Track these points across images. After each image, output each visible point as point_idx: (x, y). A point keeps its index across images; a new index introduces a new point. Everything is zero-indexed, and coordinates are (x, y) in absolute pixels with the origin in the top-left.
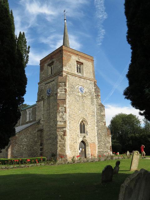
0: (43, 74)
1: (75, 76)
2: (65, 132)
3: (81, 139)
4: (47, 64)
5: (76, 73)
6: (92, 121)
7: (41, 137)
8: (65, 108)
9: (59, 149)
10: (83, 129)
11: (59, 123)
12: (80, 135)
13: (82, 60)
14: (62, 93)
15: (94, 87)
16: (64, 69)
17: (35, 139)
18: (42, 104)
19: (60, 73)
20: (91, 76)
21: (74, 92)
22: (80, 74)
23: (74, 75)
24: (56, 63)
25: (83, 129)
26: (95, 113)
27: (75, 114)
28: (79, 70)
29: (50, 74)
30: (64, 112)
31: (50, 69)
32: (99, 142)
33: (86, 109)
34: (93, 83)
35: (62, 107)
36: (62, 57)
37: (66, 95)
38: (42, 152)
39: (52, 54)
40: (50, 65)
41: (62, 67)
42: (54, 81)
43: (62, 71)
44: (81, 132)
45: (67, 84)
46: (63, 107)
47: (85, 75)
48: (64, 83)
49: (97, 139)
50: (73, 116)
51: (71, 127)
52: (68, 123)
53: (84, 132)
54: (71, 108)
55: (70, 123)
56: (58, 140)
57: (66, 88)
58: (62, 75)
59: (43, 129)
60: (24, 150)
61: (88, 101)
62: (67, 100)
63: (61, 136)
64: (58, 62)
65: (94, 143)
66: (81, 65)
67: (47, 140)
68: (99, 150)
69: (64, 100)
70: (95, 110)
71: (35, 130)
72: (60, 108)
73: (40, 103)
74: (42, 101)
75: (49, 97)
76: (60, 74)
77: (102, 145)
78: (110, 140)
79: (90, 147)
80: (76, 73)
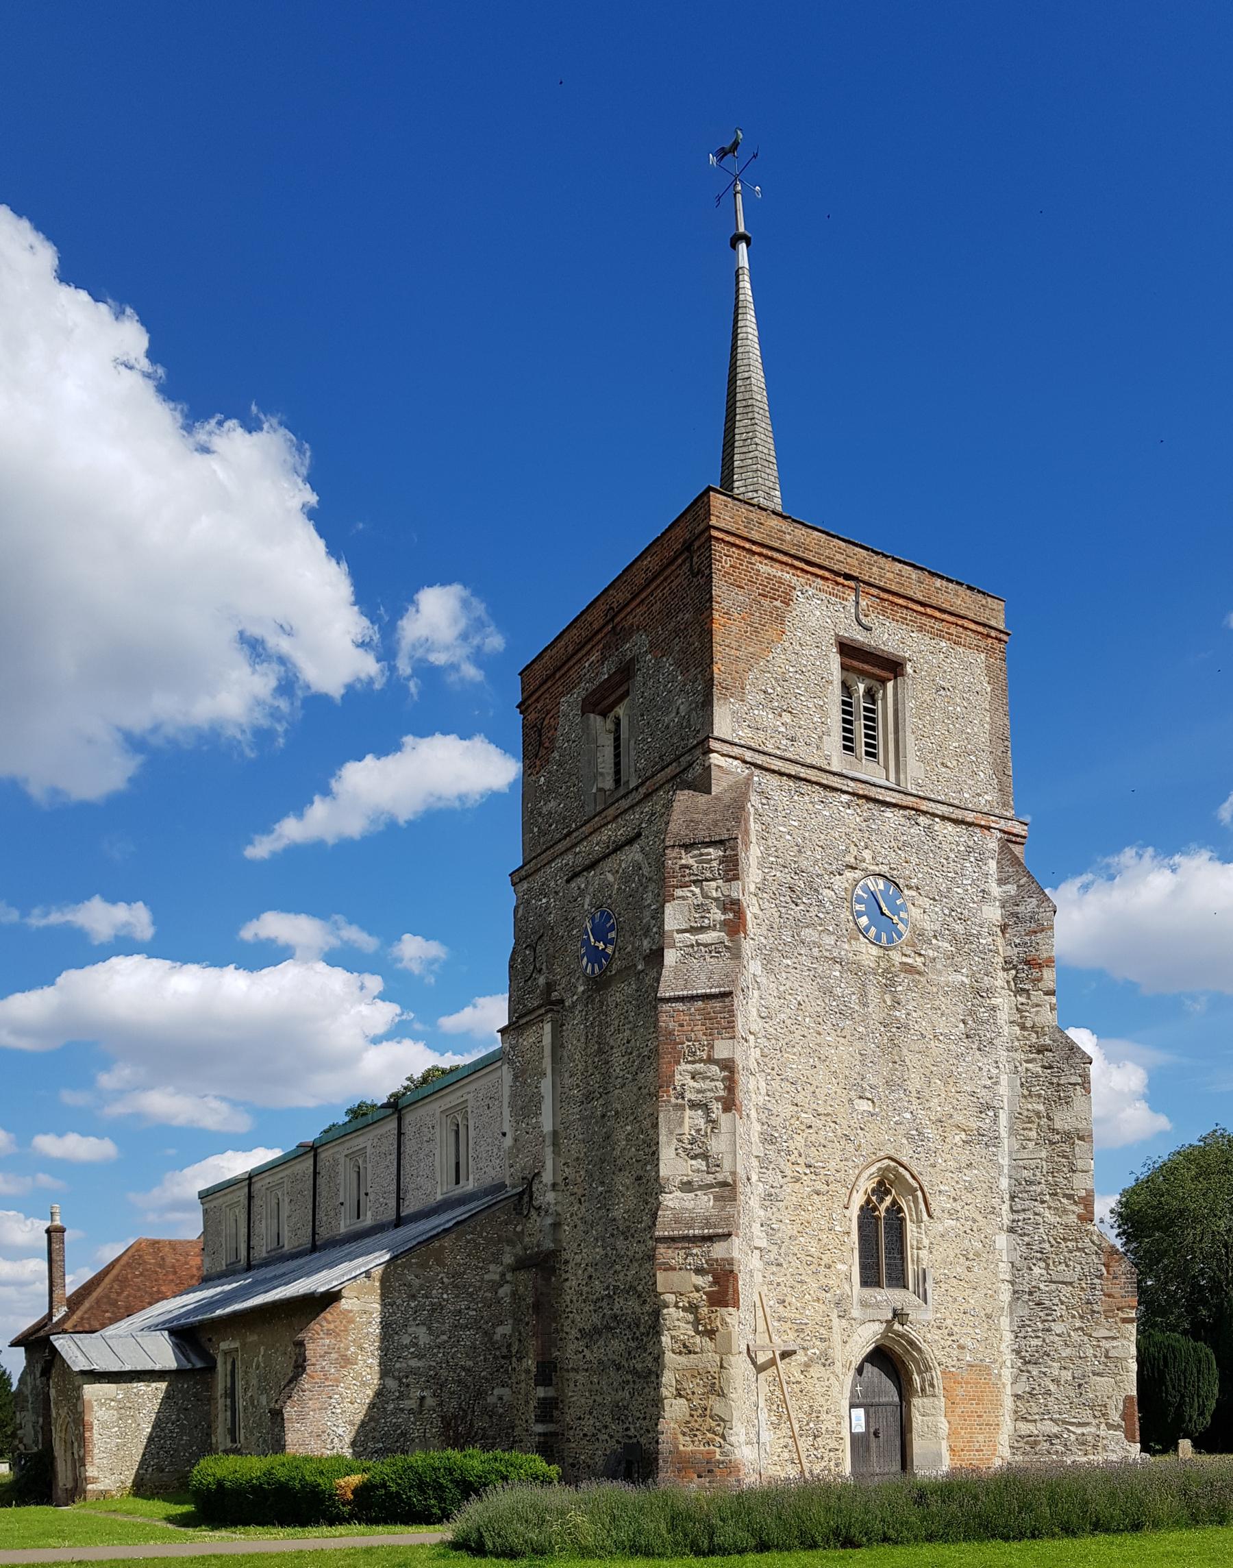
0: (550, 790)
1: (824, 783)
2: (723, 1286)
3: (866, 1337)
4: (578, 695)
5: (838, 761)
6: (970, 1189)
7: (544, 1309)
8: (728, 1066)
9: (674, 1410)
10: (883, 1248)
11: (672, 1200)
12: (864, 1304)
13: (888, 635)
14: (704, 937)
15: (1001, 882)
16: (724, 722)
17: (500, 1330)
18: (547, 1052)
19: (686, 759)
20: (980, 790)
21: (808, 934)
22: (871, 771)
23: (812, 775)
24: (659, 674)
25: (883, 1248)
26: (1003, 1118)
27: (818, 1123)
28: (863, 728)
29: (608, 784)
30: (716, 1107)
31: (607, 741)
32: (1027, 1361)
33: (915, 1082)
34: (993, 845)
35: (699, 1067)
36: (704, 604)
37: (736, 954)
38: (551, 1427)
39: (621, 596)
40: (600, 702)
41: (707, 704)
42: (636, 847)
43: (702, 744)
44: (870, 1278)
45: (752, 856)
46: (710, 1060)
47: (915, 773)
48: (714, 853)
49: (1008, 1336)
50: (799, 1141)
51: (788, 1229)
52: (751, 1199)
53: (898, 1280)
54: (790, 1074)
55: (770, 1198)
56: (666, 1340)
57: (735, 890)
58: (703, 785)
59: (554, 1254)
60: (411, 1411)
61: (936, 1018)
62: (748, 1013)
63: (693, 1308)
64: (668, 664)
65: (981, 1369)
66: (883, 682)
67: (590, 1335)
68: (1025, 1428)
69: (719, 1004)
70: (1003, 1089)
71: (496, 1260)
72: (682, 1073)
73: (528, 1040)
74: (548, 1027)
75: (599, 984)
76: (690, 776)
77: (1053, 1387)
78: (1127, 1346)
79: (942, 1402)
80: (838, 761)
